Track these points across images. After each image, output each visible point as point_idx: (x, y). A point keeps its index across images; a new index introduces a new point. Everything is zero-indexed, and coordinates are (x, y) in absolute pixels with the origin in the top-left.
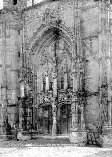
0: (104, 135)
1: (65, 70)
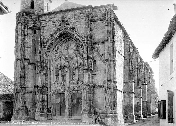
0: (109, 117)
1: (76, 66)
